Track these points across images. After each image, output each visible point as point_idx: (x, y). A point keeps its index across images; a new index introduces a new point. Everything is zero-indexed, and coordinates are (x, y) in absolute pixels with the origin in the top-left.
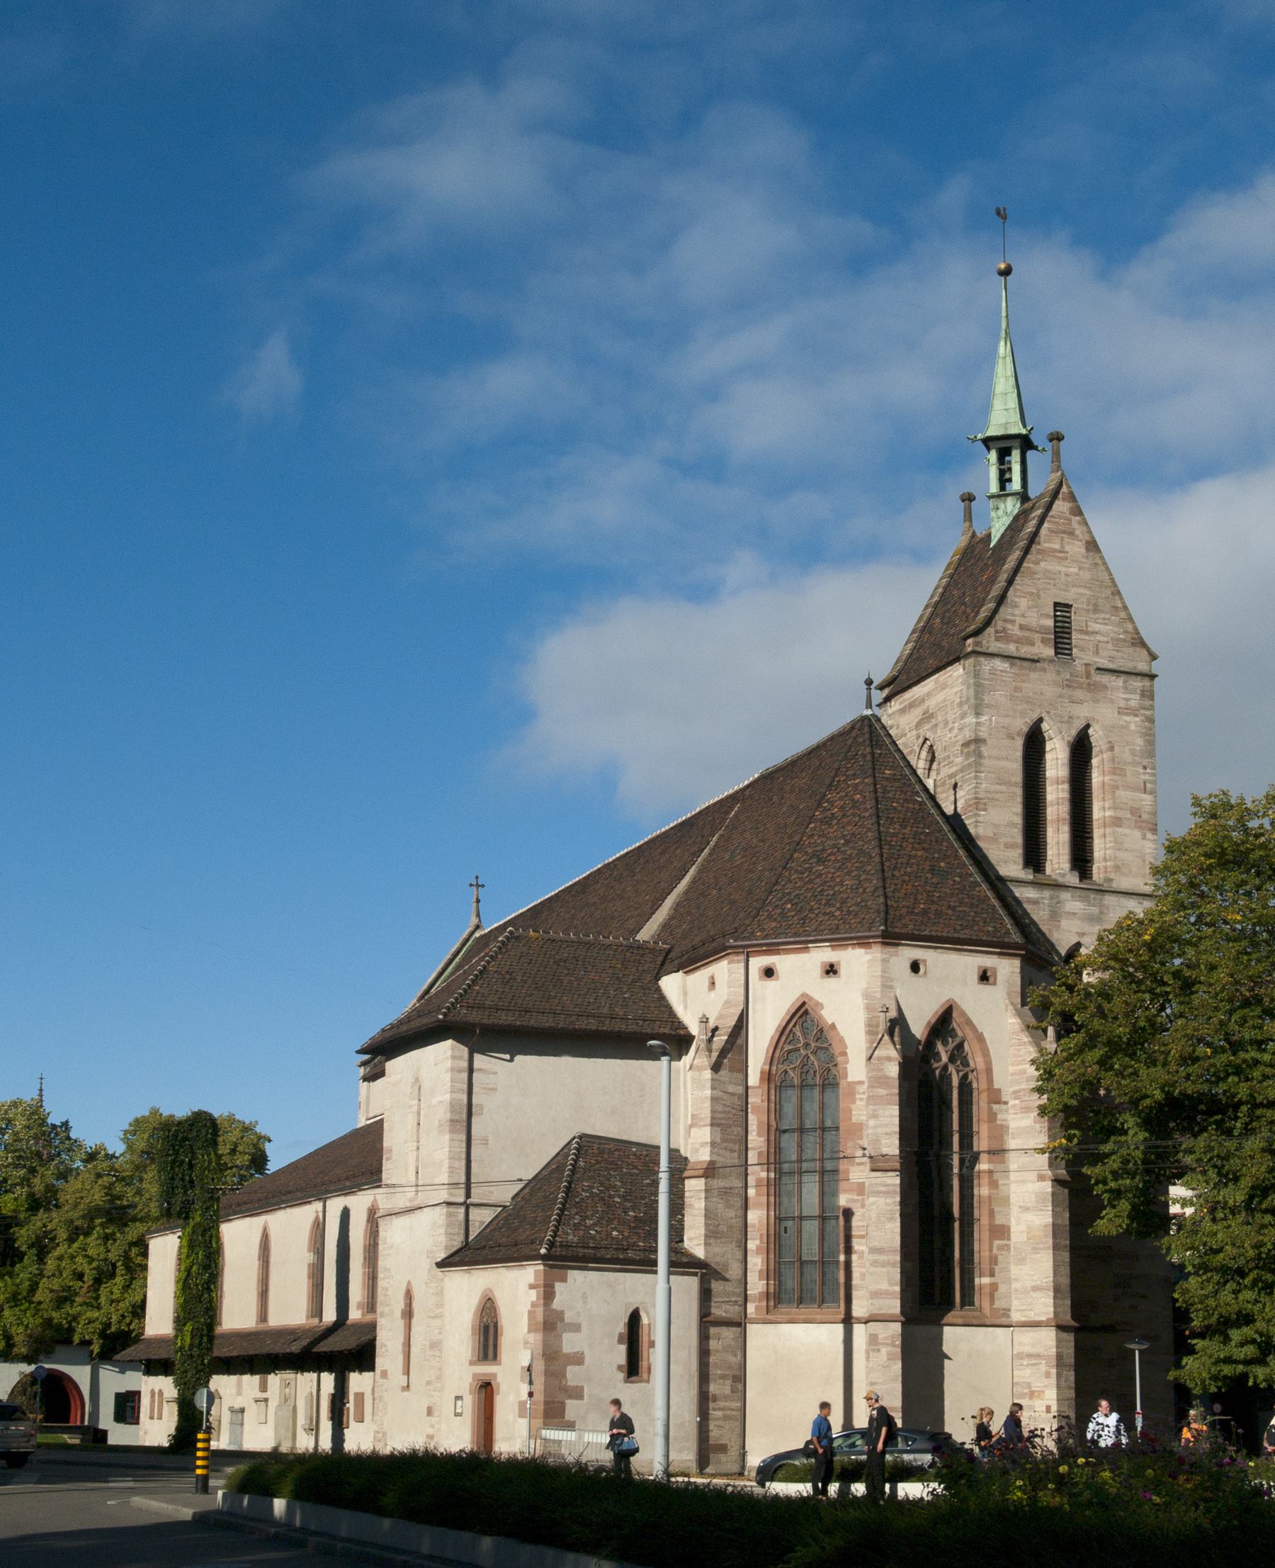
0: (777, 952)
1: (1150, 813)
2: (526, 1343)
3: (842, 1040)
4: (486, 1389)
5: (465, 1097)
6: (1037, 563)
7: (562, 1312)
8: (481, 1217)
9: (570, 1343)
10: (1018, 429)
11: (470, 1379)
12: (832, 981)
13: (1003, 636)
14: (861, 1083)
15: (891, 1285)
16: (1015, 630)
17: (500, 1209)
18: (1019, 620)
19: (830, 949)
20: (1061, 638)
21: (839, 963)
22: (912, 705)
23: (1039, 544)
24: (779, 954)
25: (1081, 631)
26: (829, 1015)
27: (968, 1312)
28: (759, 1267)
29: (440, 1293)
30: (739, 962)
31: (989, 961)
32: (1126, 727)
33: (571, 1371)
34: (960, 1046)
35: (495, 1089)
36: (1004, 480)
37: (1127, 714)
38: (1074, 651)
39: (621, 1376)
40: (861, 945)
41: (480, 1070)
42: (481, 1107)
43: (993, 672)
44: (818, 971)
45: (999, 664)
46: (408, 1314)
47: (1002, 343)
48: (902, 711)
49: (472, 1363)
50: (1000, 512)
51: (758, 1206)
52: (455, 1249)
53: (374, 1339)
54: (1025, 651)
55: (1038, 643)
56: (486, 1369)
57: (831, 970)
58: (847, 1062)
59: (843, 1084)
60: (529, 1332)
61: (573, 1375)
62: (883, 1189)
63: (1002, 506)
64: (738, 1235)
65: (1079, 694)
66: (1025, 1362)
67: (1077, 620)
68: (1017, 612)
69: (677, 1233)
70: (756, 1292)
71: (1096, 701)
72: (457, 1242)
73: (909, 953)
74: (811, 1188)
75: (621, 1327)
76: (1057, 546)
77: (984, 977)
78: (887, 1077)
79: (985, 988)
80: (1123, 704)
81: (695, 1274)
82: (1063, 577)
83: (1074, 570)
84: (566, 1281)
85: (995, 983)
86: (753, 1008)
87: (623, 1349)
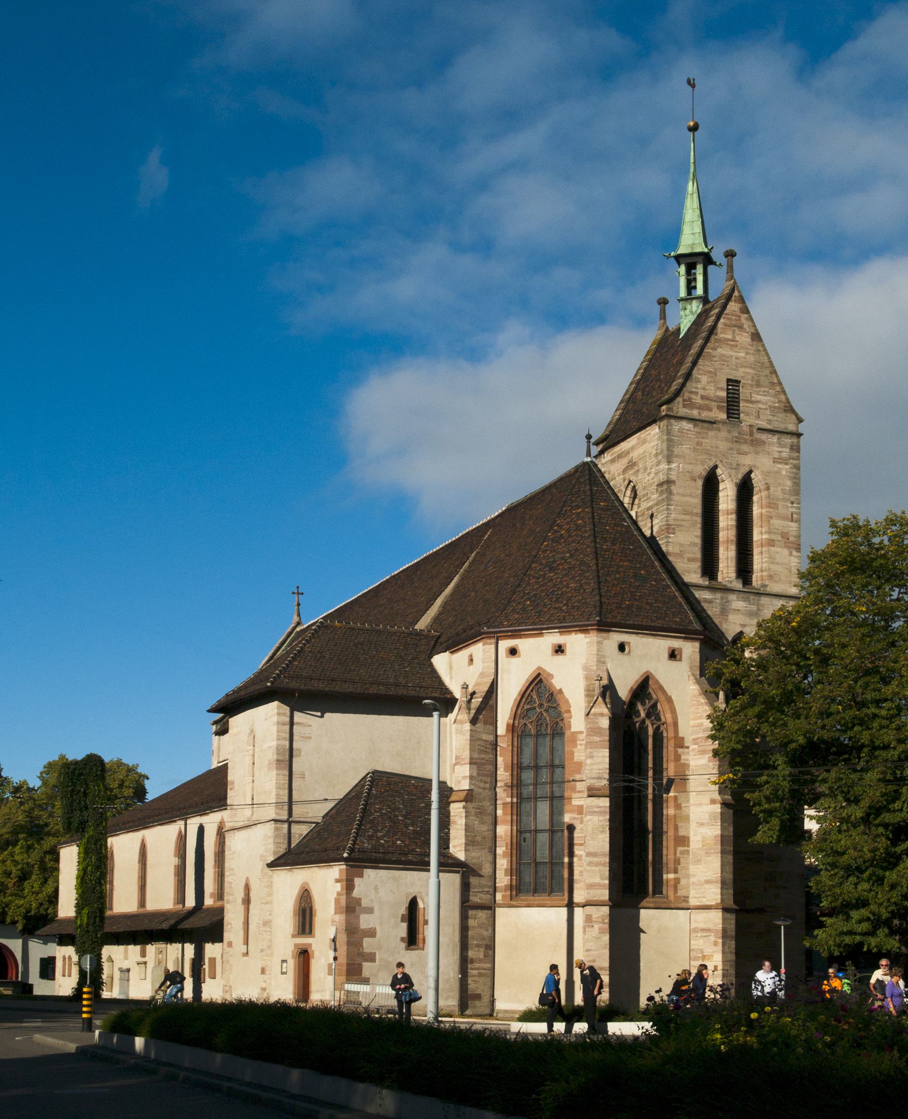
0: (520, 637)
1: (795, 537)
2: (333, 921)
3: (567, 701)
4: (304, 955)
5: (287, 743)
6: (715, 349)
7: (360, 899)
8: (300, 831)
9: (365, 921)
10: (701, 248)
11: (293, 948)
12: (560, 658)
13: (689, 404)
14: (581, 732)
15: (602, 879)
16: (697, 400)
17: (314, 825)
18: (701, 392)
19: (558, 634)
20: (732, 405)
21: (565, 645)
22: (620, 456)
23: (716, 334)
24: (521, 638)
25: (747, 401)
26: (557, 683)
27: (658, 899)
28: (505, 867)
29: (270, 886)
30: (491, 644)
31: (676, 644)
32: (779, 472)
33: (367, 942)
34: (655, 706)
35: (310, 738)
36: (691, 287)
37: (780, 463)
38: (742, 415)
39: (403, 945)
40: (582, 631)
41: (299, 723)
42: (300, 750)
43: (681, 431)
44: (549, 650)
45: (686, 425)
46: (247, 901)
47: (690, 183)
48: (613, 461)
49: (293, 936)
50: (687, 312)
51: (504, 822)
52: (281, 854)
53: (223, 919)
54: (705, 415)
55: (715, 409)
56: (304, 941)
57: (559, 650)
58: (571, 717)
59: (567, 733)
60: (335, 913)
61: (368, 944)
62: (597, 810)
63: (689, 307)
64: (489, 844)
65: (745, 448)
66: (699, 935)
67: (744, 392)
68: (699, 386)
69: (444, 842)
70: (503, 884)
71: (757, 453)
72: (282, 850)
73: (617, 637)
74: (543, 808)
75: (403, 910)
76: (730, 337)
77: (673, 655)
78: (600, 728)
79: (674, 663)
80: (776, 455)
81: (458, 872)
82: (734, 359)
83: (742, 354)
84: (362, 877)
85: (680, 660)
86: (502, 679)
87: (405, 925)
